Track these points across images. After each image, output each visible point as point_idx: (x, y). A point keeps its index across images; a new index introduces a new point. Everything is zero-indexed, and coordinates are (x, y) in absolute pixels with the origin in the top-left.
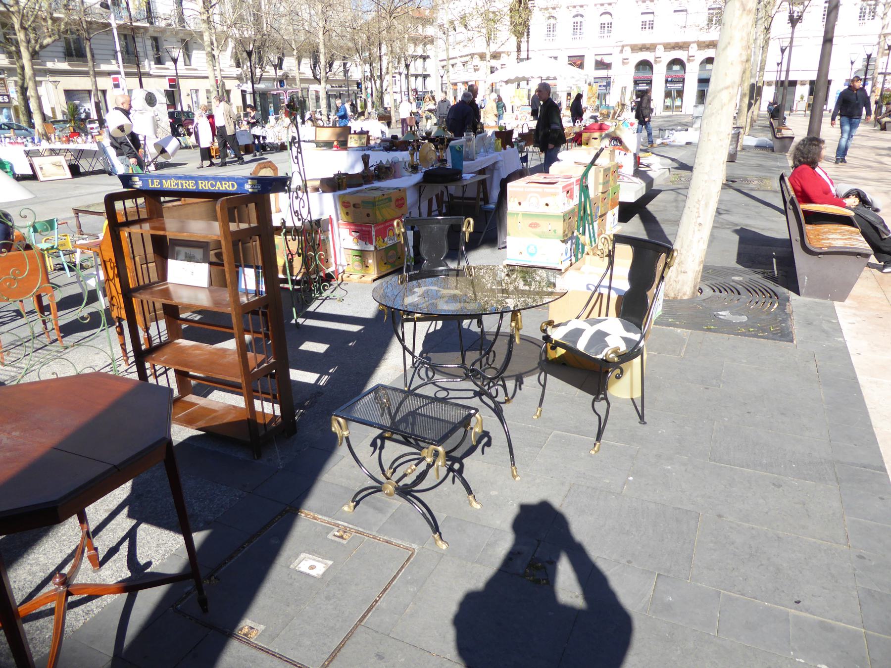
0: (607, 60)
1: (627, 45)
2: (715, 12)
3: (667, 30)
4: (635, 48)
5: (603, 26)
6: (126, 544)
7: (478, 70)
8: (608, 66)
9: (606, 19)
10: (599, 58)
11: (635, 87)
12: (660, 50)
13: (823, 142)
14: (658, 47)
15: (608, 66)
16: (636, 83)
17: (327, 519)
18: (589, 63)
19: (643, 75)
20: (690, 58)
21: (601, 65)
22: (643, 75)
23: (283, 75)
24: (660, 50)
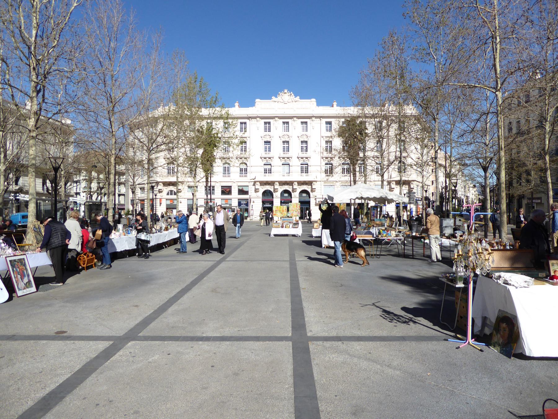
0: (245, 189)
1: (258, 181)
2: (304, 166)
3: (278, 174)
4: (263, 183)
5: (241, 170)
6: (102, 345)
7: (162, 192)
8: (246, 193)
9: (268, 167)
10: (241, 188)
11: (263, 205)
12: (277, 186)
13: (64, 282)
14: (276, 183)
15: (246, 193)
16: (264, 202)
17: (504, 207)
18: (235, 191)
19: (268, 198)
20: (294, 190)
21: (242, 192)
22: (268, 198)
23: (19, 189)
24: (277, 186)
